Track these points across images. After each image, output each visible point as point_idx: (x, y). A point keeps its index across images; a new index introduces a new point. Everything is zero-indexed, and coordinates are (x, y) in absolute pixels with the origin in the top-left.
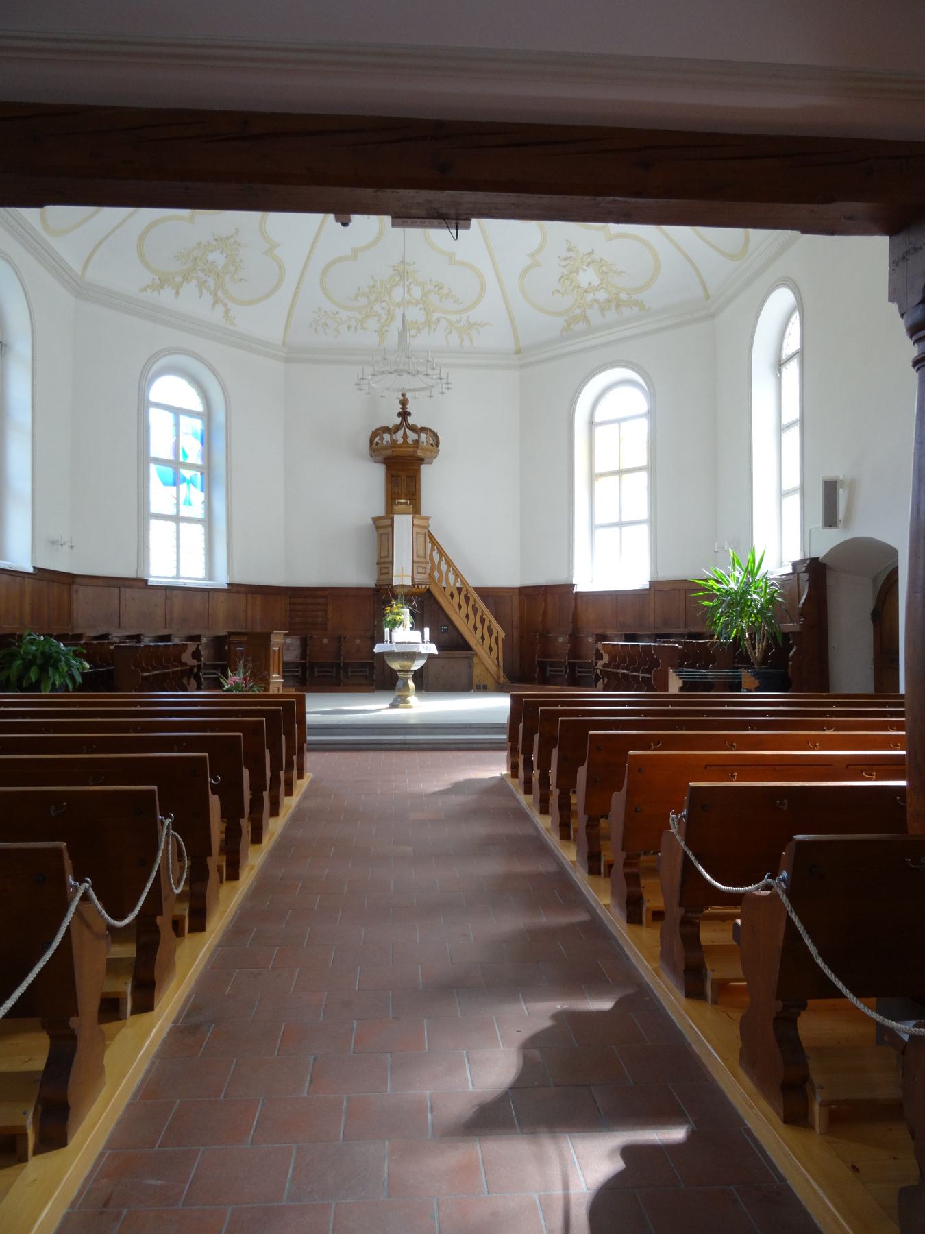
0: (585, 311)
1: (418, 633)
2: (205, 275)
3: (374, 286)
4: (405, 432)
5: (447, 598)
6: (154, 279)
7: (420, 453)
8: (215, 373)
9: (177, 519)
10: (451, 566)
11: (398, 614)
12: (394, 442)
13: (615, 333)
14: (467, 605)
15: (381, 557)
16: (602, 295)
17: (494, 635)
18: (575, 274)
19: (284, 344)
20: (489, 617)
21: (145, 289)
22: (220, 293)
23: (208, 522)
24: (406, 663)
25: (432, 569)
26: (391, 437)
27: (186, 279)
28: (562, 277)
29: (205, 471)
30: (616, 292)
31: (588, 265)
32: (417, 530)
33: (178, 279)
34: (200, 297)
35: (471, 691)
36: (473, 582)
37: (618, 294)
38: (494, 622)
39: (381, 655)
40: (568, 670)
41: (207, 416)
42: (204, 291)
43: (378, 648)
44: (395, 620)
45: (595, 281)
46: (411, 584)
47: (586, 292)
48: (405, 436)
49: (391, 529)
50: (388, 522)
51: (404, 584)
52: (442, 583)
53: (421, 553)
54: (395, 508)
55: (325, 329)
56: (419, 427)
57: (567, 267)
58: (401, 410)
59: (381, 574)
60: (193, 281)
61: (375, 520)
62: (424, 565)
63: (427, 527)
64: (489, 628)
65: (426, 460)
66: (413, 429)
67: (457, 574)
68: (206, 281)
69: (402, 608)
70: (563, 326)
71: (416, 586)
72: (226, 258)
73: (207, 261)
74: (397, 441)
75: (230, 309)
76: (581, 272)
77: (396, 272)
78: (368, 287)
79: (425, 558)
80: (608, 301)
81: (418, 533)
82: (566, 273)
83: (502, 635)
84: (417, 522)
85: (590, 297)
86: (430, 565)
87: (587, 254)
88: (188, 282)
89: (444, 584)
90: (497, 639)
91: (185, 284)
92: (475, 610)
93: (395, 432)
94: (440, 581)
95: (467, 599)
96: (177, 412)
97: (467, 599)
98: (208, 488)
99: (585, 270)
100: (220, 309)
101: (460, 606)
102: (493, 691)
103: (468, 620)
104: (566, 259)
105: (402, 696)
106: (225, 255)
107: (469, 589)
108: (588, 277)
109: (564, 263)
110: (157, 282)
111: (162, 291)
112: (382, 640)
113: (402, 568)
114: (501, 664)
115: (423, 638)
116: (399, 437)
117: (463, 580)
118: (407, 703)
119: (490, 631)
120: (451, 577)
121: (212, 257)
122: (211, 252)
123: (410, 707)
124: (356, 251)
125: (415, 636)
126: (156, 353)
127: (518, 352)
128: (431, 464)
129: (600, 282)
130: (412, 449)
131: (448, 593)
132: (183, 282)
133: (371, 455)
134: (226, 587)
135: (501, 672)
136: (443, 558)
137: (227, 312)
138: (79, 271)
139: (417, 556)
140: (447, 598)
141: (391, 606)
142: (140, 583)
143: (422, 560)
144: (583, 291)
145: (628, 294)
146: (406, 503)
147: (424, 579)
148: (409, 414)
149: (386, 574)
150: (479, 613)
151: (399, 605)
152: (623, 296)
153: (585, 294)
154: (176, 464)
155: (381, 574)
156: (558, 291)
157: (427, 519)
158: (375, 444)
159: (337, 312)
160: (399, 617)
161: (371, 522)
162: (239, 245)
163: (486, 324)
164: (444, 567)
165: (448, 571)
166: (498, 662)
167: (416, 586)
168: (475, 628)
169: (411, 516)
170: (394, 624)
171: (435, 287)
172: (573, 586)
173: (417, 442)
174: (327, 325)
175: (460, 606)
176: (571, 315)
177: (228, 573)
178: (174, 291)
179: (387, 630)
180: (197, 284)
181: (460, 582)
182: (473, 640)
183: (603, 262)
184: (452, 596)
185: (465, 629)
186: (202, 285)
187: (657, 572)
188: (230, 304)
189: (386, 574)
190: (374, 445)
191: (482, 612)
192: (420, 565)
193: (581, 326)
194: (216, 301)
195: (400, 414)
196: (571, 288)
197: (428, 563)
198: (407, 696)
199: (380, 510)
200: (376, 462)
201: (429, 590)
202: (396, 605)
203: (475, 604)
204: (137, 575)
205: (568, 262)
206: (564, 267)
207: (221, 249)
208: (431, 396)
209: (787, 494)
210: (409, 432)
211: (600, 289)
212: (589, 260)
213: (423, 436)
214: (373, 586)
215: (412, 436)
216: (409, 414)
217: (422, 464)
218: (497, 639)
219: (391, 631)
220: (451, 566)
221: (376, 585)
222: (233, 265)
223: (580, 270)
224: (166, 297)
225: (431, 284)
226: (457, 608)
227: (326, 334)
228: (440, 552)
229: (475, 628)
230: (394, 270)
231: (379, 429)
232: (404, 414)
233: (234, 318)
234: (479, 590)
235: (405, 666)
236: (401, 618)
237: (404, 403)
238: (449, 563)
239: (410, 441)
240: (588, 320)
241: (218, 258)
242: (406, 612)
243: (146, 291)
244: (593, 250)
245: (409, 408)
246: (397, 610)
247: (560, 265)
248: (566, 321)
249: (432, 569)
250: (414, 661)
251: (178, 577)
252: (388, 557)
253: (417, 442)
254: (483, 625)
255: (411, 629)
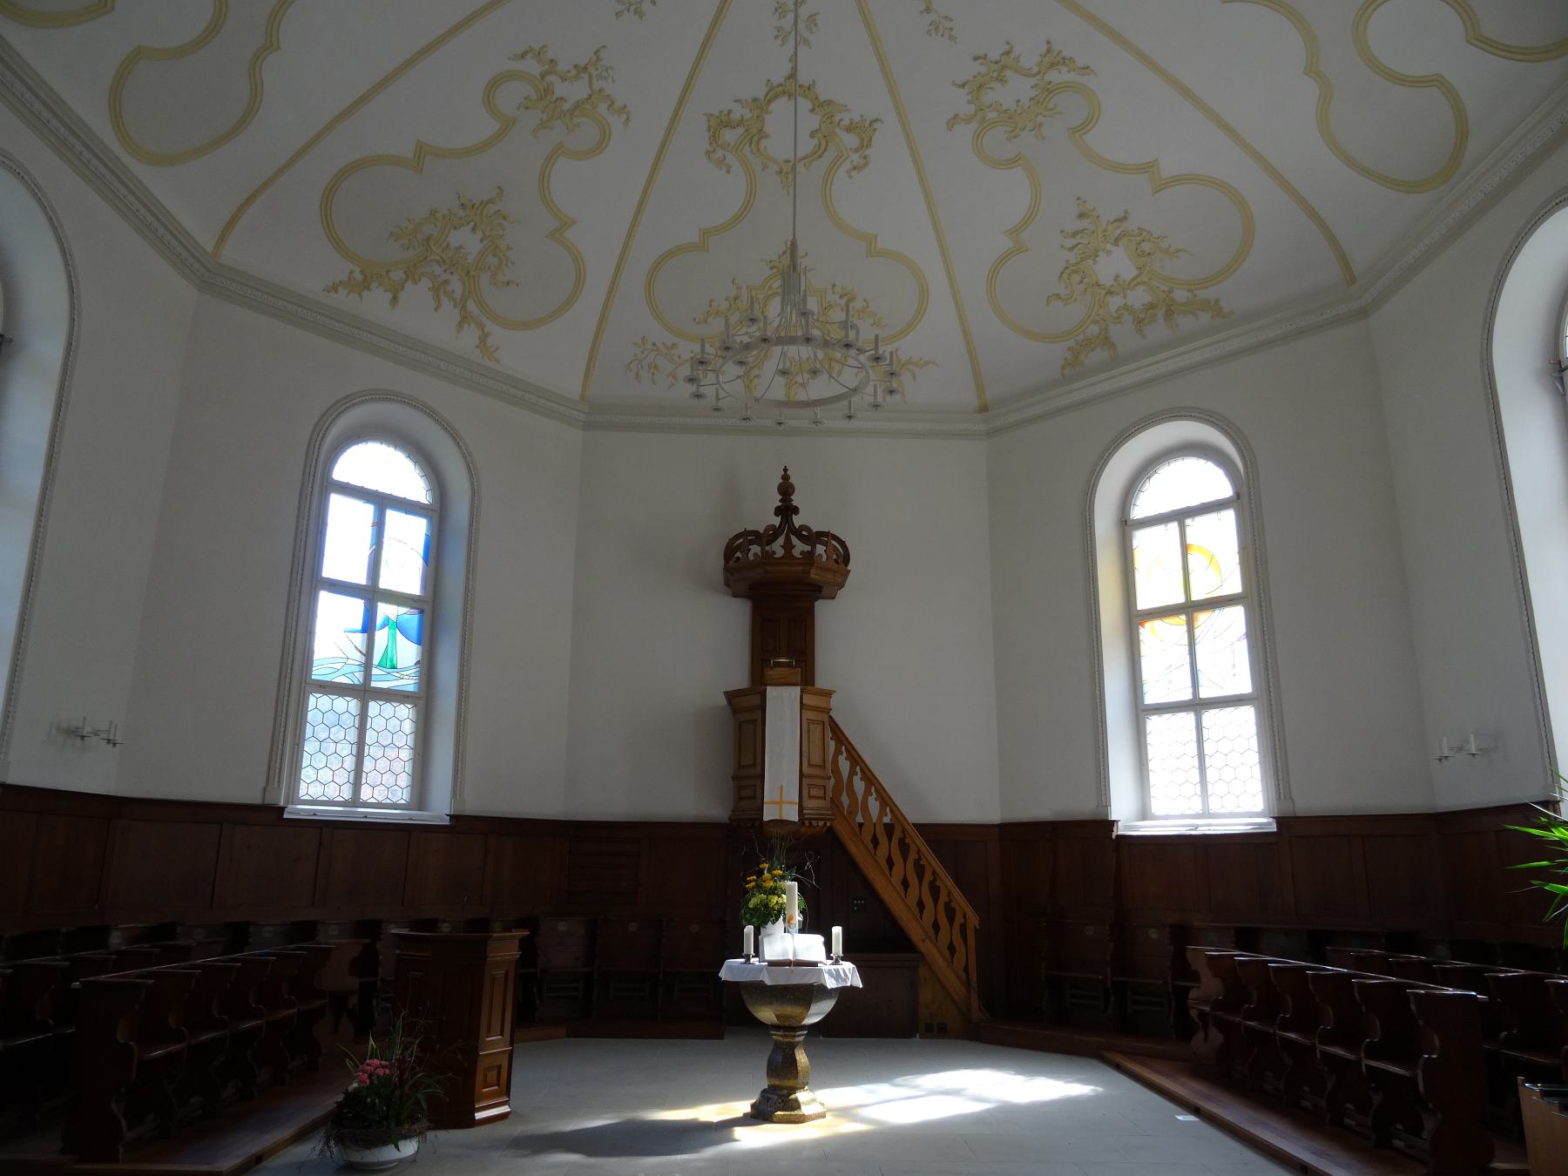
0: (1106, 330)
1: (818, 940)
2: (445, 271)
3: (736, 298)
4: (788, 540)
5: (866, 847)
6: (352, 272)
7: (814, 575)
8: (455, 438)
9: (364, 693)
10: (872, 784)
11: (774, 891)
12: (767, 557)
13: (1166, 359)
14: (890, 841)
15: (740, 767)
16: (1139, 297)
17: (959, 920)
18: (1090, 262)
19: (583, 397)
20: (947, 882)
21: (335, 288)
22: (471, 306)
23: (424, 700)
24: (790, 1010)
25: (837, 790)
26: (762, 549)
27: (411, 274)
28: (1066, 268)
29: (428, 609)
30: (1166, 289)
31: (1116, 242)
32: (809, 715)
33: (397, 275)
34: (436, 310)
35: (915, 1037)
36: (914, 815)
37: (1170, 292)
38: (957, 894)
39: (736, 987)
40: (1112, 999)
41: (438, 513)
42: (443, 298)
43: (731, 970)
44: (766, 906)
45: (1128, 271)
46: (795, 818)
47: (1110, 293)
48: (788, 546)
49: (760, 712)
50: (755, 700)
51: (784, 818)
52: (856, 817)
53: (816, 759)
54: (770, 673)
55: (653, 374)
56: (814, 531)
57: (1075, 250)
58: (780, 504)
59: (741, 799)
60: (424, 279)
61: (731, 696)
62: (821, 782)
63: (827, 710)
64: (948, 906)
65: (825, 591)
66: (798, 533)
67: (885, 800)
68: (446, 282)
69: (783, 878)
70: (1066, 359)
71: (807, 822)
72: (481, 240)
73: (448, 246)
74: (774, 553)
75: (488, 334)
76: (1102, 256)
77: (774, 270)
78: (727, 299)
79: (824, 768)
80: (1152, 306)
81: (811, 721)
82: (1073, 261)
83: (974, 920)
84: (808, 700)
85: (1115, 302)
86: (832, 781)
87: (1115, 221)
88: (415, 283)
89: (860, 819)
90: (963, 928)
91: (409, 285)
92: (920, 870)
93: (770, 542)
94: (852, 813)
95: (904, 848)
96: (382, 502)
97: (904, 848)
98: (428, 639)
99: (1109, 253)
100: (471, 335)
101: (890, 863)
102: (957, 1038)
103: (875, 848)
104: (1074, 235)
105: (782, 1088)
106: (479, 235)
107: (907, 827)
108: (1114, 264)
109: (1071, 242)
110: (359, 277)
111: (365, 293)
112: (738, 952)
113: (782, 786)
114: (974, 978)
115: (829, 948)
116: (777, 548)
117: (896, 812)
118: (793, 1109)
119: (951, 914)
120: (874, 805)
121: (458, 237)
122: (455, 228)
123: (801, 1120)
124: (706, 234)
125: (810, 947)
126: (346, 397)
127: (984, 409)
128: (834, 598)
129: (1137, 272)
130: (801, 568)
131: (867, 837)
132: (406, 281)
133: (727, 584)
134: (446, 821)
135: (974, 997)
136: (873, 790)
137: (484, 338)
138: (209, 248)
139: (810, 765)
140: (866, 847)
141: (760, 873)
142: (266, 818)
143: (817, 772)
144: (1103, 292)
145: (1189, 291)
146: (788, 665)
147: (818, 809)
148: (796, 510)
149: (750, 798)
150: (928, 877)
151: (776, 872)
152: (1180, 295)
153: (1109, 298)
154: (371, 594)
155: (741, 799)
156: (1058, 296)
157: (828, 694)
158: (734, 559)
159: (674, 346)
160: (775, 899)
161: (723, 701)
162: (505, 218)
163: (928, 363)
164: (859, 785)
165: (852, 773)
166: (967, 975)
167: (807, 822)
168: (921, 905)
169: (799, 688)
170: (767, 915)
171: (841, 297)
172: (1113, 823)
173: (810, 555)
174: (656, 366)
175: (890, 863)
176: (1081, 337)
177: (454, 794)
178: (389, 296)
179: (749, 929)
180: (431, 286)
181: (889, 816)
182: (916, 931)
183: (1144, 234)
184: (875, 841)
185: (901, 910)
186: (439, 289)
187: (1291, 798)
188: (490, 326)
189: (750, 798)
190: (731, 562)
191: (934, 873)
192: (814, 781)
193: (1098, 356)
194: (465, 318)
195: (778, 511)
196: (1082, 288)
197: (829, 778)
198: (794, 1090)
199: (739, 678)
200: (735, 596)
201: (831, 831)
202: (770, 871)
203: (920, 858)
204: (264, 799)
205: (1078, 239)
206: (1072, 249)
207: (472, 224)
208: (850, 417)
209: (408, 697)
210: (794, 540)
211: (1133, 287)
212: (1119, 231)
213: (820, 549)
214: (727, 821)
215: (799, 547)
216: (796, 510)
217: (817, 598)
218: (963, 928)
219: (757, 933)
220: (872, 784)
221: (730, 819)
222: (494, 255)
223: (1101, 254)
224: (374, 304)
225: (833, 293)
226: (885, 866)
227: (654, 382)
228: (868, 777)
229: (921, 905)
230: (771, 269)
231: (745, 533)
232: (787, 510)
233: (496, 349)
234: (923, 828)
235: (788, 1017)
236: (780, 900)
237: (786, 489)
238: (870, 779)
239: (796, 553)
240: (1113, 345)
241: (467, 241)
242: (793, 887)
243: (336, 291)
244: (1126, 212)
245: (796, 500)
246: (771, 884)
247: (1062, 246)
248: (1070, 349)
249: (837, 790)
250: (808, 1008)
251: (355, 801)
252: (754, 765)
253: (810, 555)
254: (905, 857)
255: (802, 931)
